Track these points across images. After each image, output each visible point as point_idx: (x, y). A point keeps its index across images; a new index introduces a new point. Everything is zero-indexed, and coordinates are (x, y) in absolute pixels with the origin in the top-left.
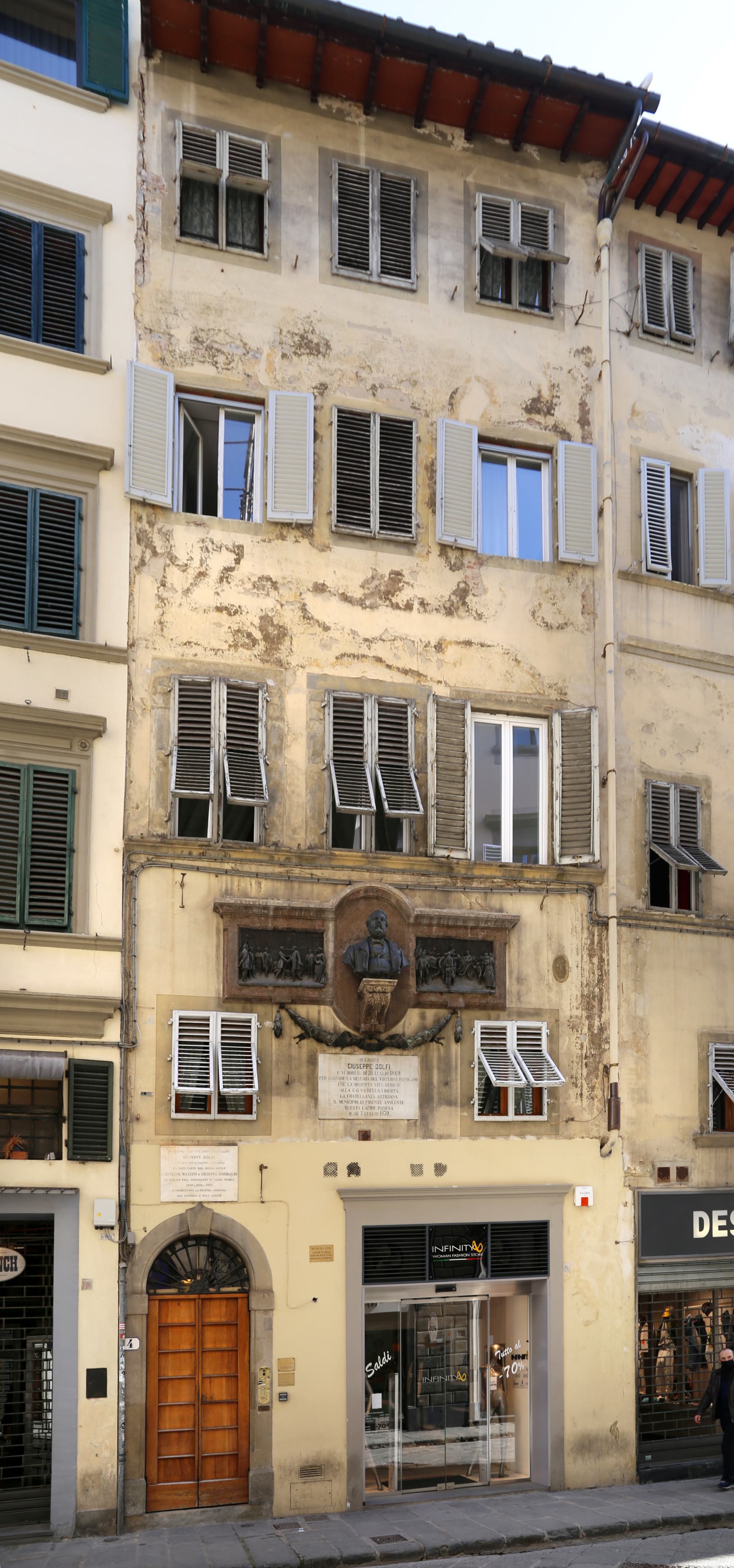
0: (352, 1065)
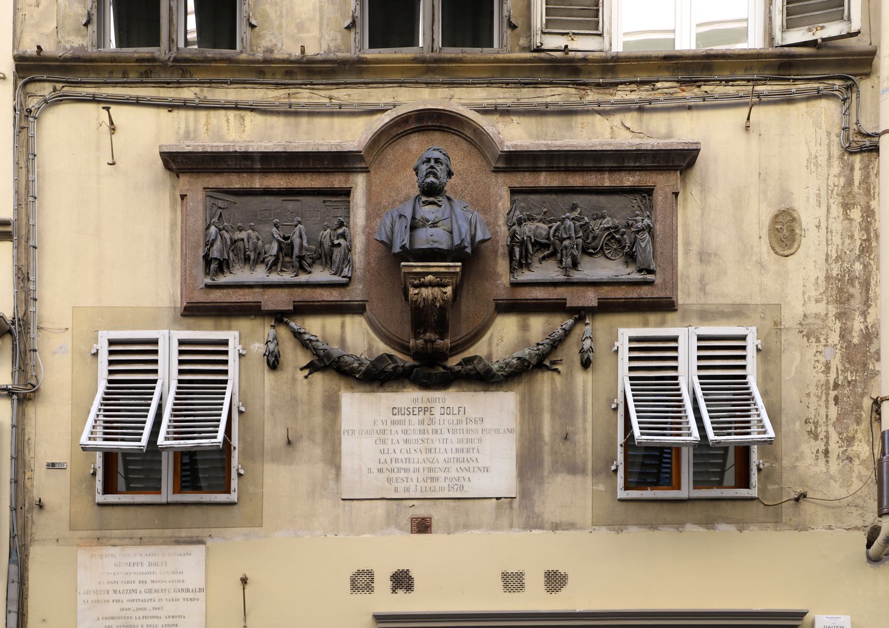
0: (400, 410)
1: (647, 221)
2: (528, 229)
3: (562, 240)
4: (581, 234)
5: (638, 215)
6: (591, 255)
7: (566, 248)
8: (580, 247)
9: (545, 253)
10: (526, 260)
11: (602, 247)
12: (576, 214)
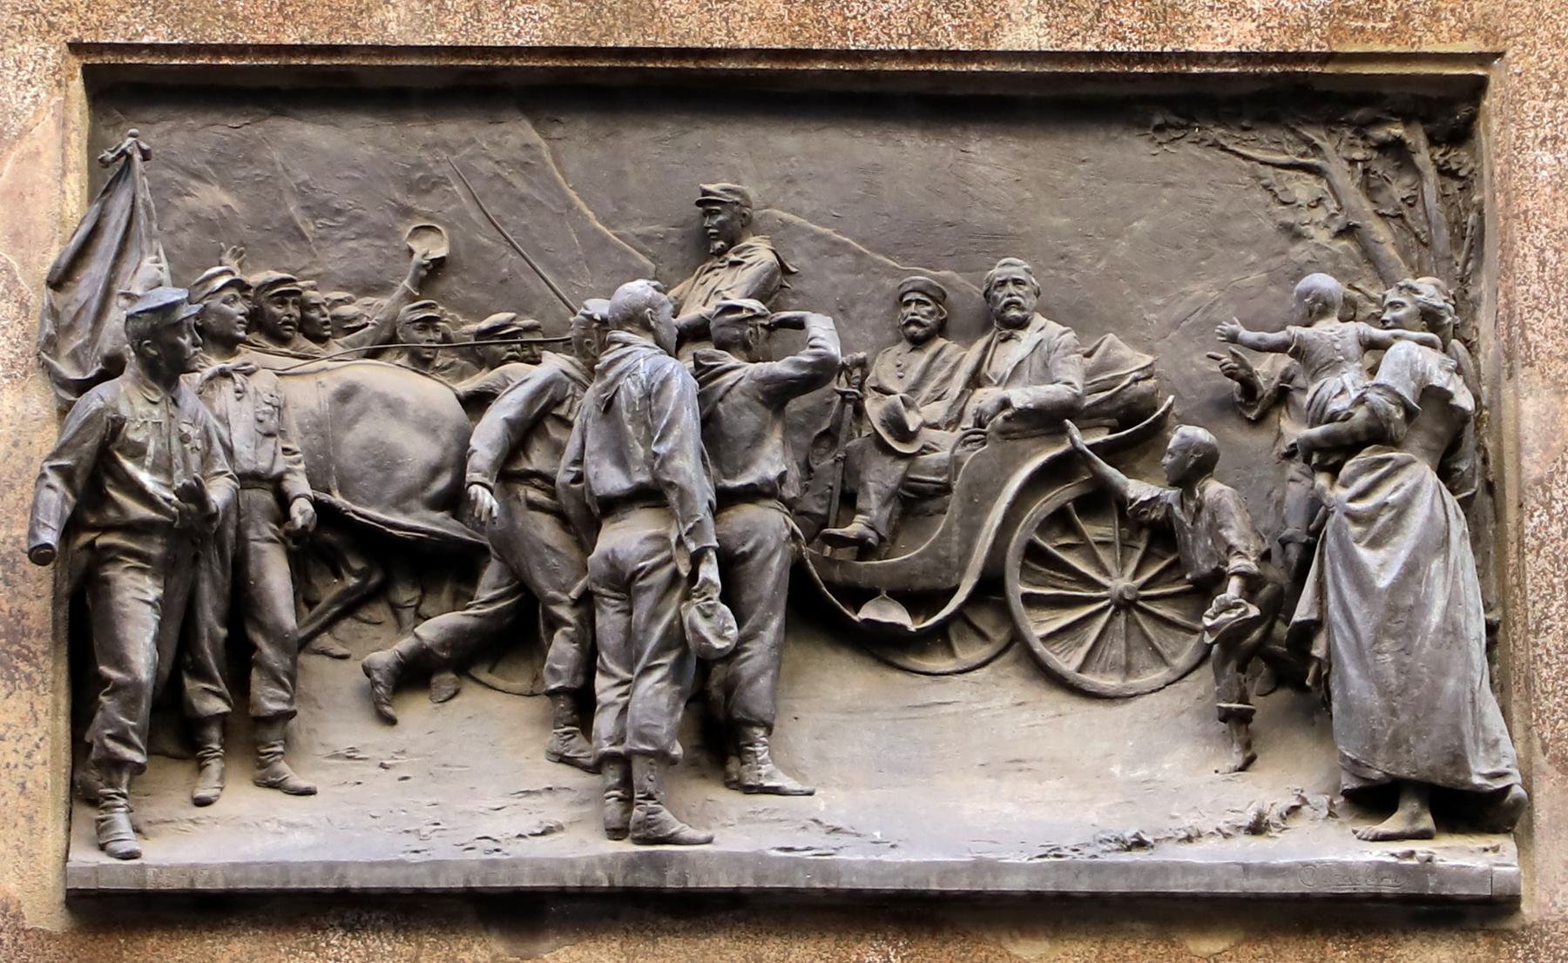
1: (1412, 360)
2: (249, 416)
3: (586, 516)
4: (771, 461)
5: (1318, 308)
6: (883, 647)
7: (624, 582)
8: (771, 578)
9: (431, 630)
10: (239, 688)
11: (991, 587)
12: (730, 287)
